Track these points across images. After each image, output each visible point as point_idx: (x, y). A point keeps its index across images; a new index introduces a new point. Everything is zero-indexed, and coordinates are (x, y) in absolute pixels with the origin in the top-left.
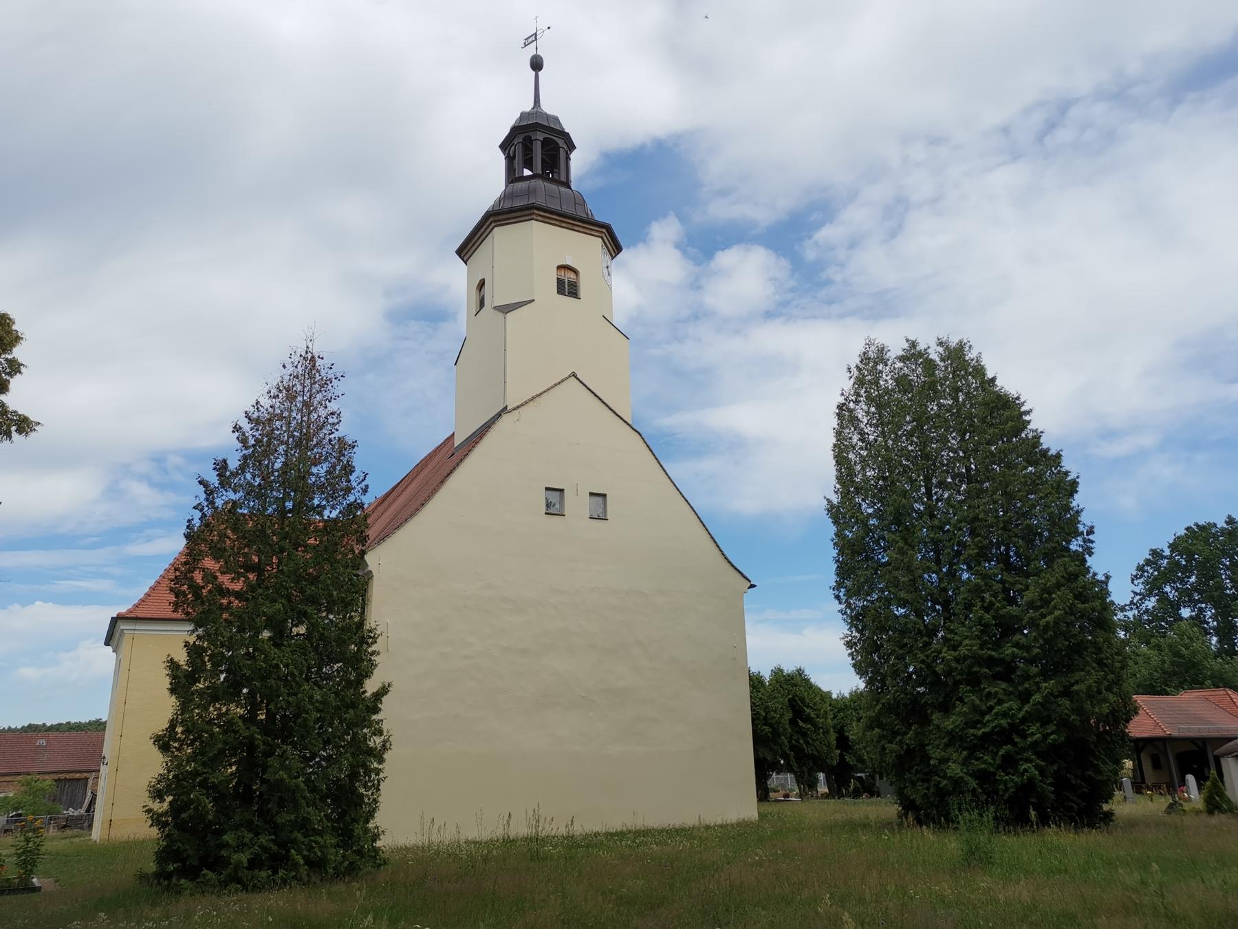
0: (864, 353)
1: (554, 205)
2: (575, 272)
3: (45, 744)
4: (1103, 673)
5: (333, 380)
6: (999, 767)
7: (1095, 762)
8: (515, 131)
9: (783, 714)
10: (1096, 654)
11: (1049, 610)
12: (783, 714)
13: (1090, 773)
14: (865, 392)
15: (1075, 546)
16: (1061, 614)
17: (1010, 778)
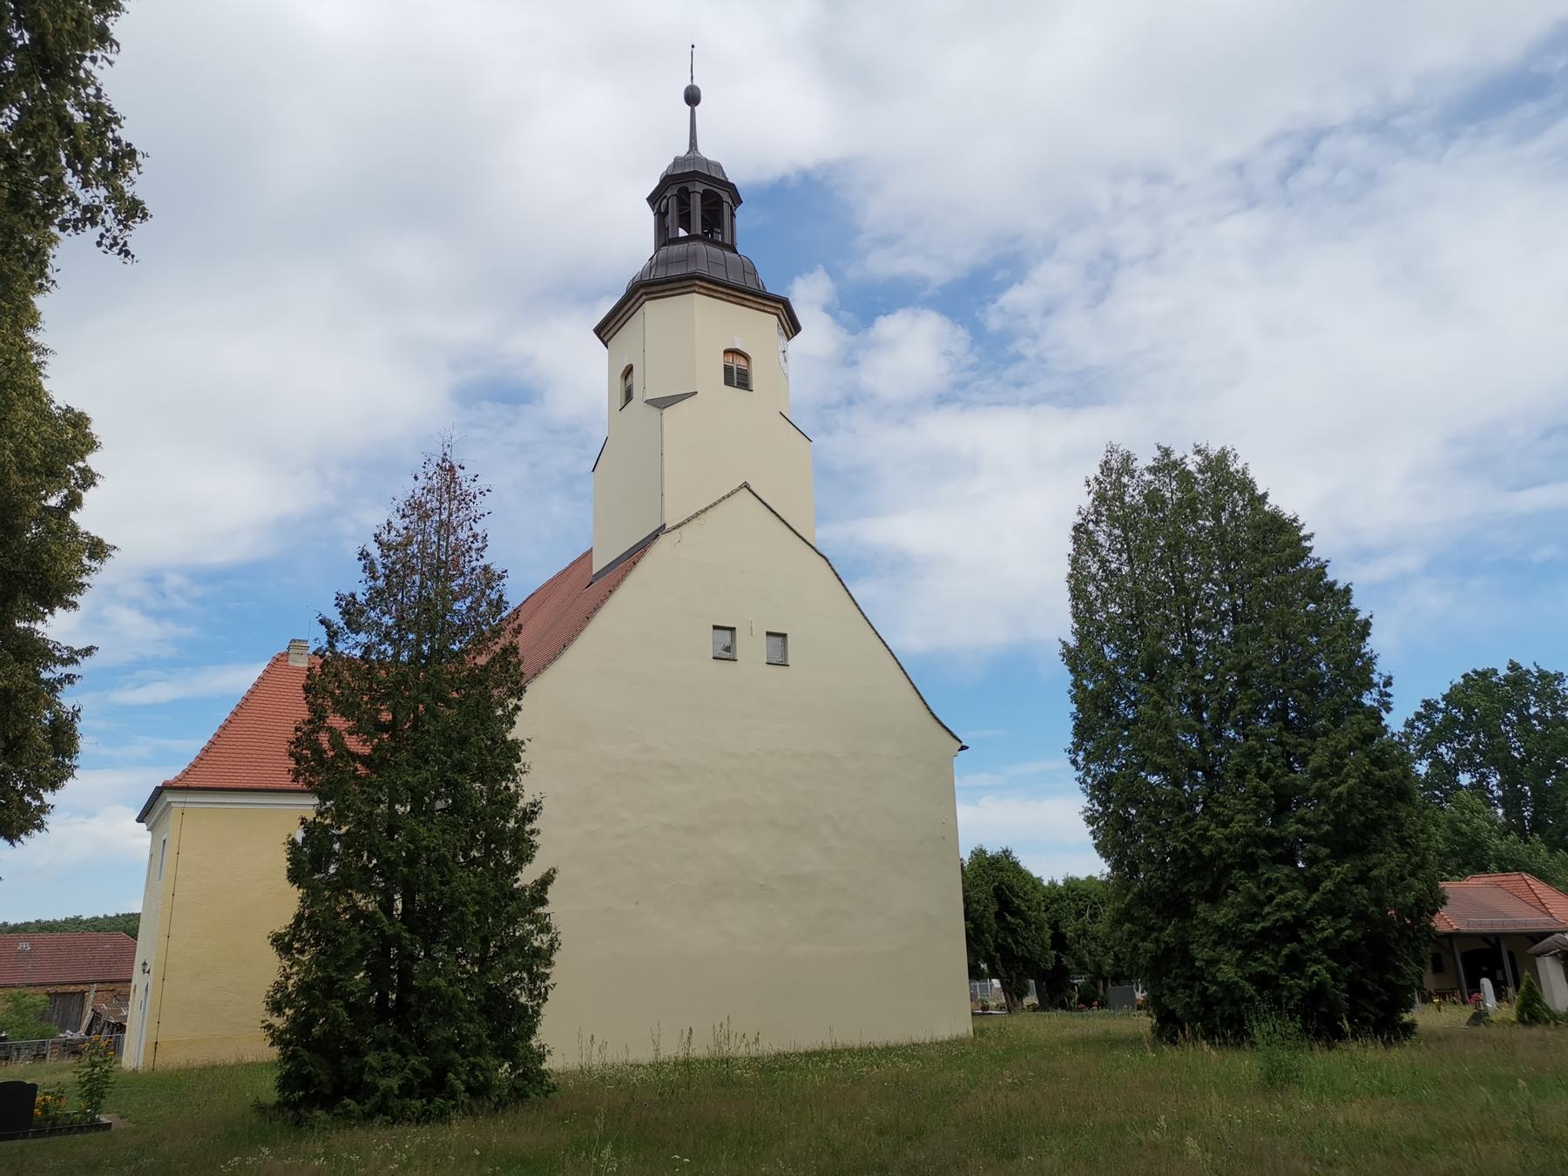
0: (1106, 462)
1: (720, 275)
2: (746, 357)
3: (29, 948)
4: (1407, 855)
5: (478, 495)
6: (1282, 970)
7: (1397, 963)
8: (667, 181)
9: (988, 906)
10: (1397, 832)
11: (1341, 779)
12: (988, 906)
13: (1390, 977)
14: (1106, 510)
15: (1368, 699)
16: (1355, 784)
17: (1296, 983)
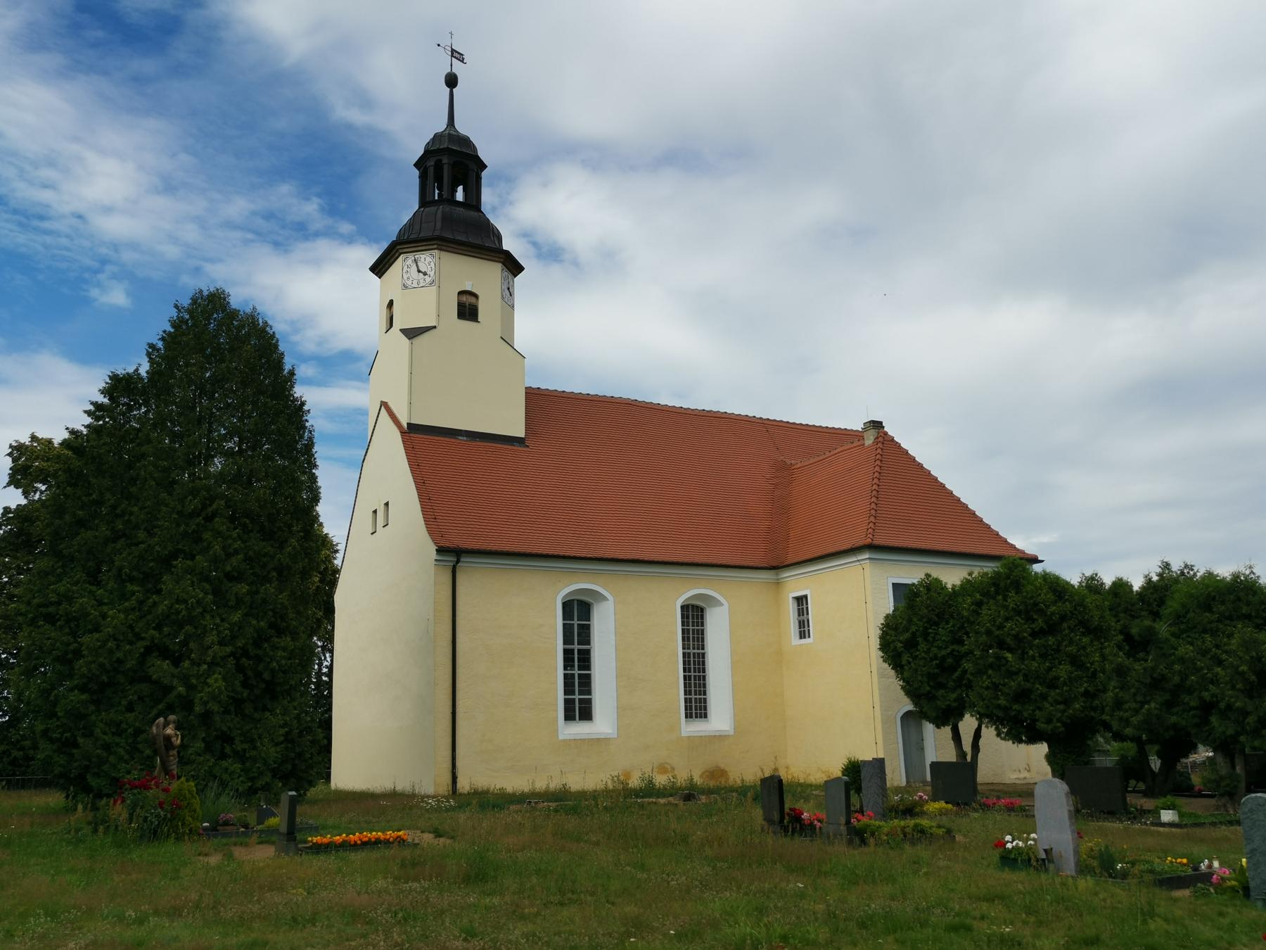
2: (476, 296)
8: (428, 153)
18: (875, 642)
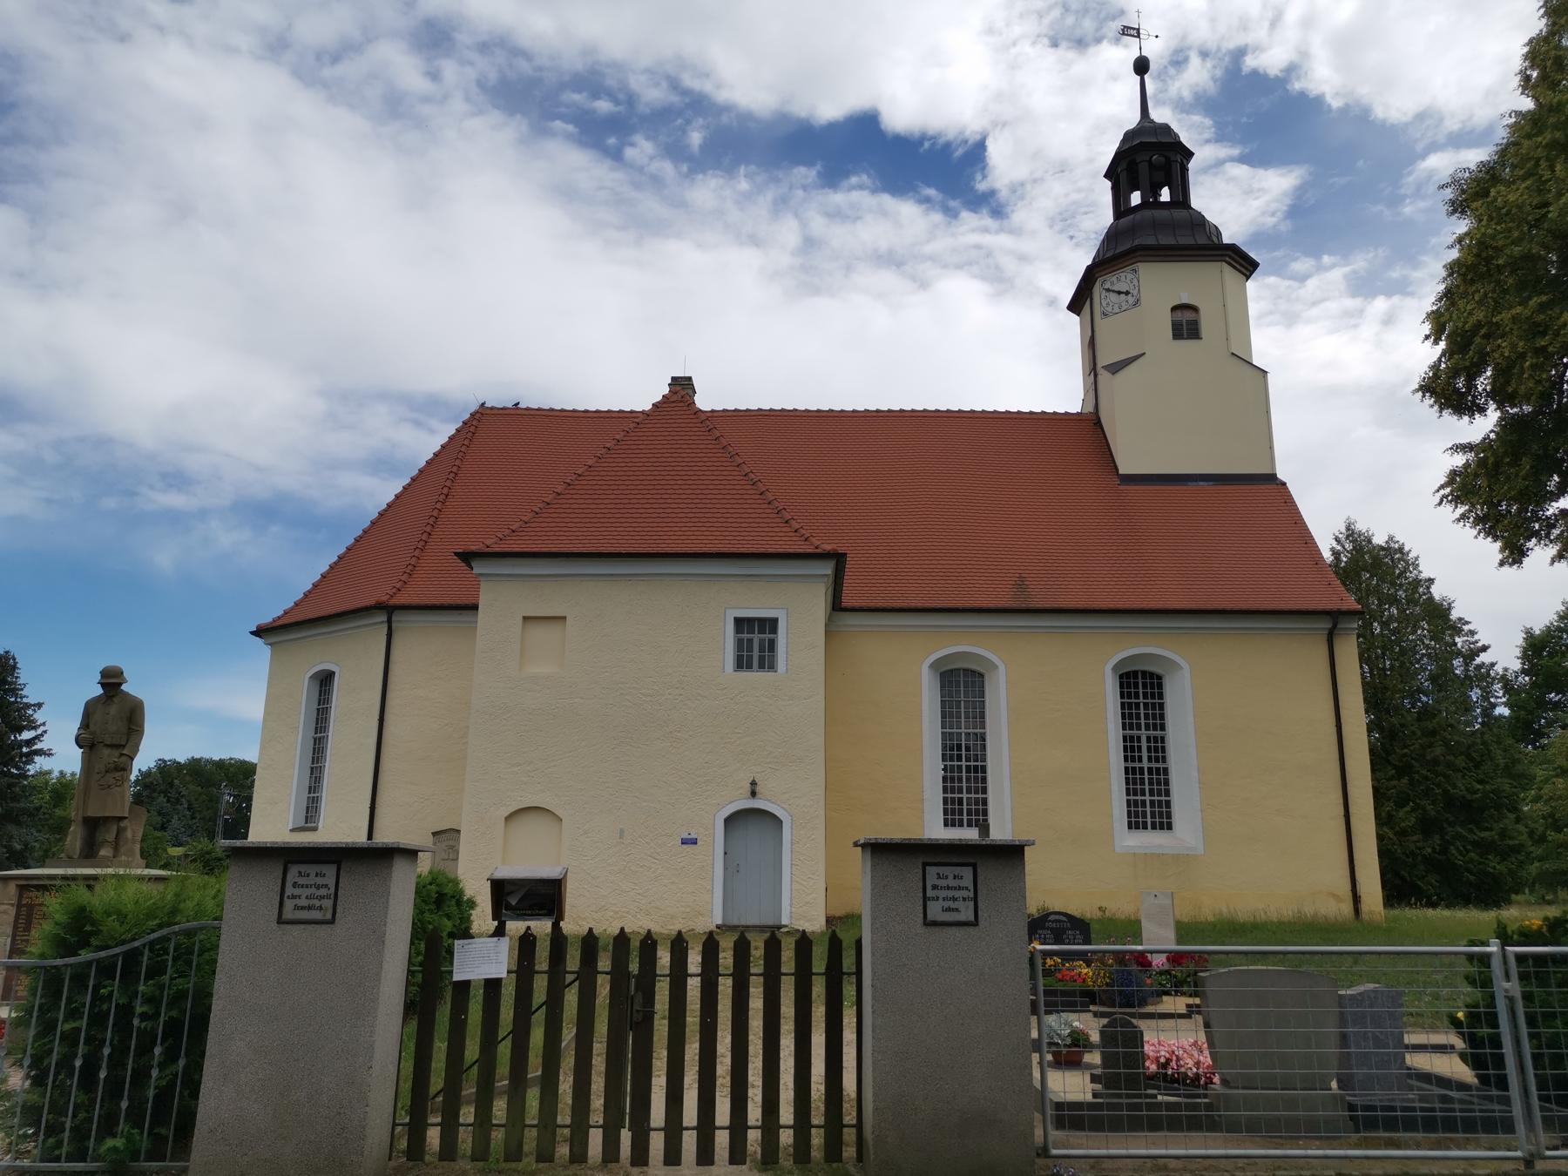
2: (1194, 309)
18: (86, 700)
